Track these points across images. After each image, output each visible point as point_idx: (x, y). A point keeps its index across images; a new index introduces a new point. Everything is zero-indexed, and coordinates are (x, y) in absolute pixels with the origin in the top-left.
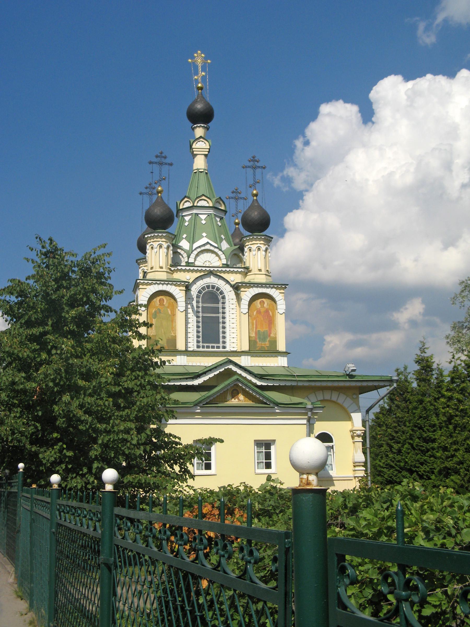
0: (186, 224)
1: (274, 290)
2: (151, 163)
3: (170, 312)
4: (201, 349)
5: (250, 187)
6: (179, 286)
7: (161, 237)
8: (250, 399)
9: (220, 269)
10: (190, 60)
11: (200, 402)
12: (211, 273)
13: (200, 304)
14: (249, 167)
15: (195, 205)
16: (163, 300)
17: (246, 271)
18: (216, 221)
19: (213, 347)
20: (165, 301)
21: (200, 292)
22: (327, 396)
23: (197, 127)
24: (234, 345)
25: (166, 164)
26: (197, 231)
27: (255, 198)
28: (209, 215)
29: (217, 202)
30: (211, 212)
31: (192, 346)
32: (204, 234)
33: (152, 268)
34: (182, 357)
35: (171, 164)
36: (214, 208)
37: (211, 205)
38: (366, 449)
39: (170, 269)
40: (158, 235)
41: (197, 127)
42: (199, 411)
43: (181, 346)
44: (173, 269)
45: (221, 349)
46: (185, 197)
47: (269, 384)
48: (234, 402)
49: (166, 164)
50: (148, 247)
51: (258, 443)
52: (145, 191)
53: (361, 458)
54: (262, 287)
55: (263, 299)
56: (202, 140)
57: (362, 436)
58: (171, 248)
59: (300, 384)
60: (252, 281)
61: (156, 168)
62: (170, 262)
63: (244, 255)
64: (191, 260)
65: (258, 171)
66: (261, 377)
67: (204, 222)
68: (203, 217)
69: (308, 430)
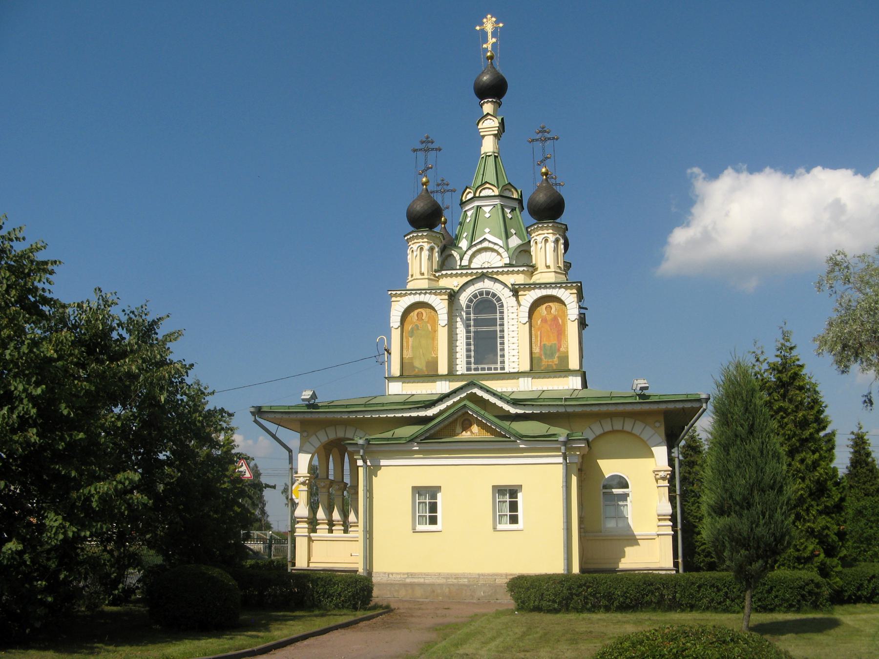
1: (563, 290)
4: (473, 372)
6: (440, 294)
7: (422, 237)
10: (478, 28)
11: (416, 437)
12: (482, 276)
13: (472, 315)
15: (477, 195)
17: (531, 269)
19: (489, 369)
20: (424, 315)
21: (471, 301)
24: (513, 365)
28: (494, 206)
30: (497, 202)
34: (444, 382)
36: (501, 196)
38: (675, 498)
39: (435, 276)
43: (443, 369)
44: (437, 275)
45: (499, 371)
46: (467, 188)
48: (466, 435)
50: (409, 251)
51: (500, 490)
53: (668, 509)
54: (546, 288)
59: (570, 410)
60: (538, 282)
62: (435, 267)
66: (515, 403)
67: (487, 215)
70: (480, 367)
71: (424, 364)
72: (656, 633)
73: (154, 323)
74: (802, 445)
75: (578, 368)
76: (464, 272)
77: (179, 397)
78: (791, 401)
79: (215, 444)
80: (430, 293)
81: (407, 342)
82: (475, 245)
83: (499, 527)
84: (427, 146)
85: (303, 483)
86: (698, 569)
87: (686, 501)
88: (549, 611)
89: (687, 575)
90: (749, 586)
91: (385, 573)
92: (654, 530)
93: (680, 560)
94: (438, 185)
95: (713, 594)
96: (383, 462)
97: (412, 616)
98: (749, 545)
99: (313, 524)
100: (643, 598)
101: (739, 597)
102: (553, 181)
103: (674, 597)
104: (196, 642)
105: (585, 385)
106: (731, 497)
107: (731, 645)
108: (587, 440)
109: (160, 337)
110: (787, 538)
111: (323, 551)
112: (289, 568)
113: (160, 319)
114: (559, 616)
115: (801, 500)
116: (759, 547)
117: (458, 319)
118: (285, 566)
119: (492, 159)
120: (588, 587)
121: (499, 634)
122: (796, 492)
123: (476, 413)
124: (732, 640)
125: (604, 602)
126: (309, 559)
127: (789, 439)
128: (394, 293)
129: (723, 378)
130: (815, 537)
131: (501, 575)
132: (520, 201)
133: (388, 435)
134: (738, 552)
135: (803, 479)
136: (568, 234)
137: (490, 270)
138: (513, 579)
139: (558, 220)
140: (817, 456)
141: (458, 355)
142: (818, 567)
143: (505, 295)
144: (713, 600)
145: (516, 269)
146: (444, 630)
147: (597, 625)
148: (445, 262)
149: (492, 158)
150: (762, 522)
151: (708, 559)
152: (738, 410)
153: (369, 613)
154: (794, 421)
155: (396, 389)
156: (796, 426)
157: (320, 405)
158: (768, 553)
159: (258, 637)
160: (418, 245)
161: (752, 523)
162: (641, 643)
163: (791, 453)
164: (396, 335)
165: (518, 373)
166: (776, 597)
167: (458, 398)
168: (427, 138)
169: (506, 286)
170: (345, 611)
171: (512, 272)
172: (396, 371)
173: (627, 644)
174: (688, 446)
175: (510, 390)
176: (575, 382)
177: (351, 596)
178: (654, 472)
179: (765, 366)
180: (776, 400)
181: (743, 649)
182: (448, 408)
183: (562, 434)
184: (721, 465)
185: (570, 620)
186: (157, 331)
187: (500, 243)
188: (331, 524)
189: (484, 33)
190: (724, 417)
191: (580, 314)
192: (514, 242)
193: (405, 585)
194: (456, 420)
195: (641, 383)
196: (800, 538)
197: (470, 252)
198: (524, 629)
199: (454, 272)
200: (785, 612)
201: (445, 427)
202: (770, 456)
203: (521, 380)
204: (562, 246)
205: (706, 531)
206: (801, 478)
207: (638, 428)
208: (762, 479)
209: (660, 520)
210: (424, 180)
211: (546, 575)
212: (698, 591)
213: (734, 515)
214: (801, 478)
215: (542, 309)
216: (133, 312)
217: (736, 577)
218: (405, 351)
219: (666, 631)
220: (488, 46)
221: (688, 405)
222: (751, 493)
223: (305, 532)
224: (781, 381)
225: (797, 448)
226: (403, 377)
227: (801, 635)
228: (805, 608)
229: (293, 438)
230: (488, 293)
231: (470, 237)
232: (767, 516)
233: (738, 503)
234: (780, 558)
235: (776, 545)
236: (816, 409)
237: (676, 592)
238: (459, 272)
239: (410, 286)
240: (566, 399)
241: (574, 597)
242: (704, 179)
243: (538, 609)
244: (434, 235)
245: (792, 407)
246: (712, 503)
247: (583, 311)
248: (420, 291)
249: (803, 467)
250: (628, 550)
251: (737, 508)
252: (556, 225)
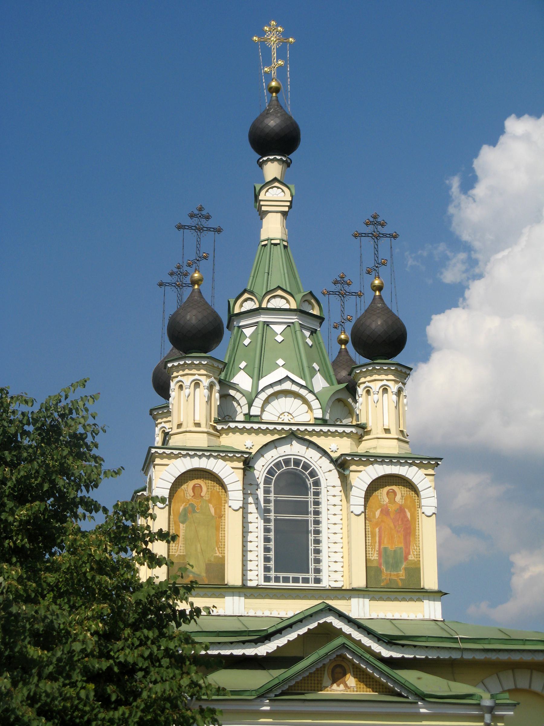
0: (247, 342)
1: (414, 468)
2: (180, 227)
3: (212, 511)
4: (272, 583)
5: (369, 273)
6: (231, 460)
7: (198, 367)
9: (310, 428)
10: (255, 38)
11: (270, 690)
12: (293, 436)
13: (272, 495)
14: (366, 235)
15: (264, 305)
17: (360, 431)
18: (304, 337)
19: (296, 580)
20: (204, 489)
21: (271, 472)
24: (338, 576)
25: (209, 229)
26: (267, 355)
29: (305, 300)
30: (294, 319)
31: (256, 578)
32: (280, 362)
33: (179, 426)
34: (236, 598)
35: (218, 230)
36: (299, 311)
37: (294, 306)
39: (215, 428)
41: (268, 160)
42: (268, 708)
43: (233, 577)
44: (219, 427)
45: (312, 585)
46: (245, 291)
47: (406, 656)
48: (336, 690)
49: (209, 229)
52: (188, 222)
54: (391, 463)
55: (394, 487)
56: (277, 184)
58: (217, 387)
59: (468, 656)
60: (372, 452)
61: (190, 235)
62: (214, 415)
63: (356, 401)
64: (255, 411)
65: (384, 242)
66: (389, 641)
67: (279, 338)
68: (278, 329)
71: (203, 567)
80: (216, 457)
160: (192, 378)
168: (201, 209)
210: (196, 275)
215: (383, 494)
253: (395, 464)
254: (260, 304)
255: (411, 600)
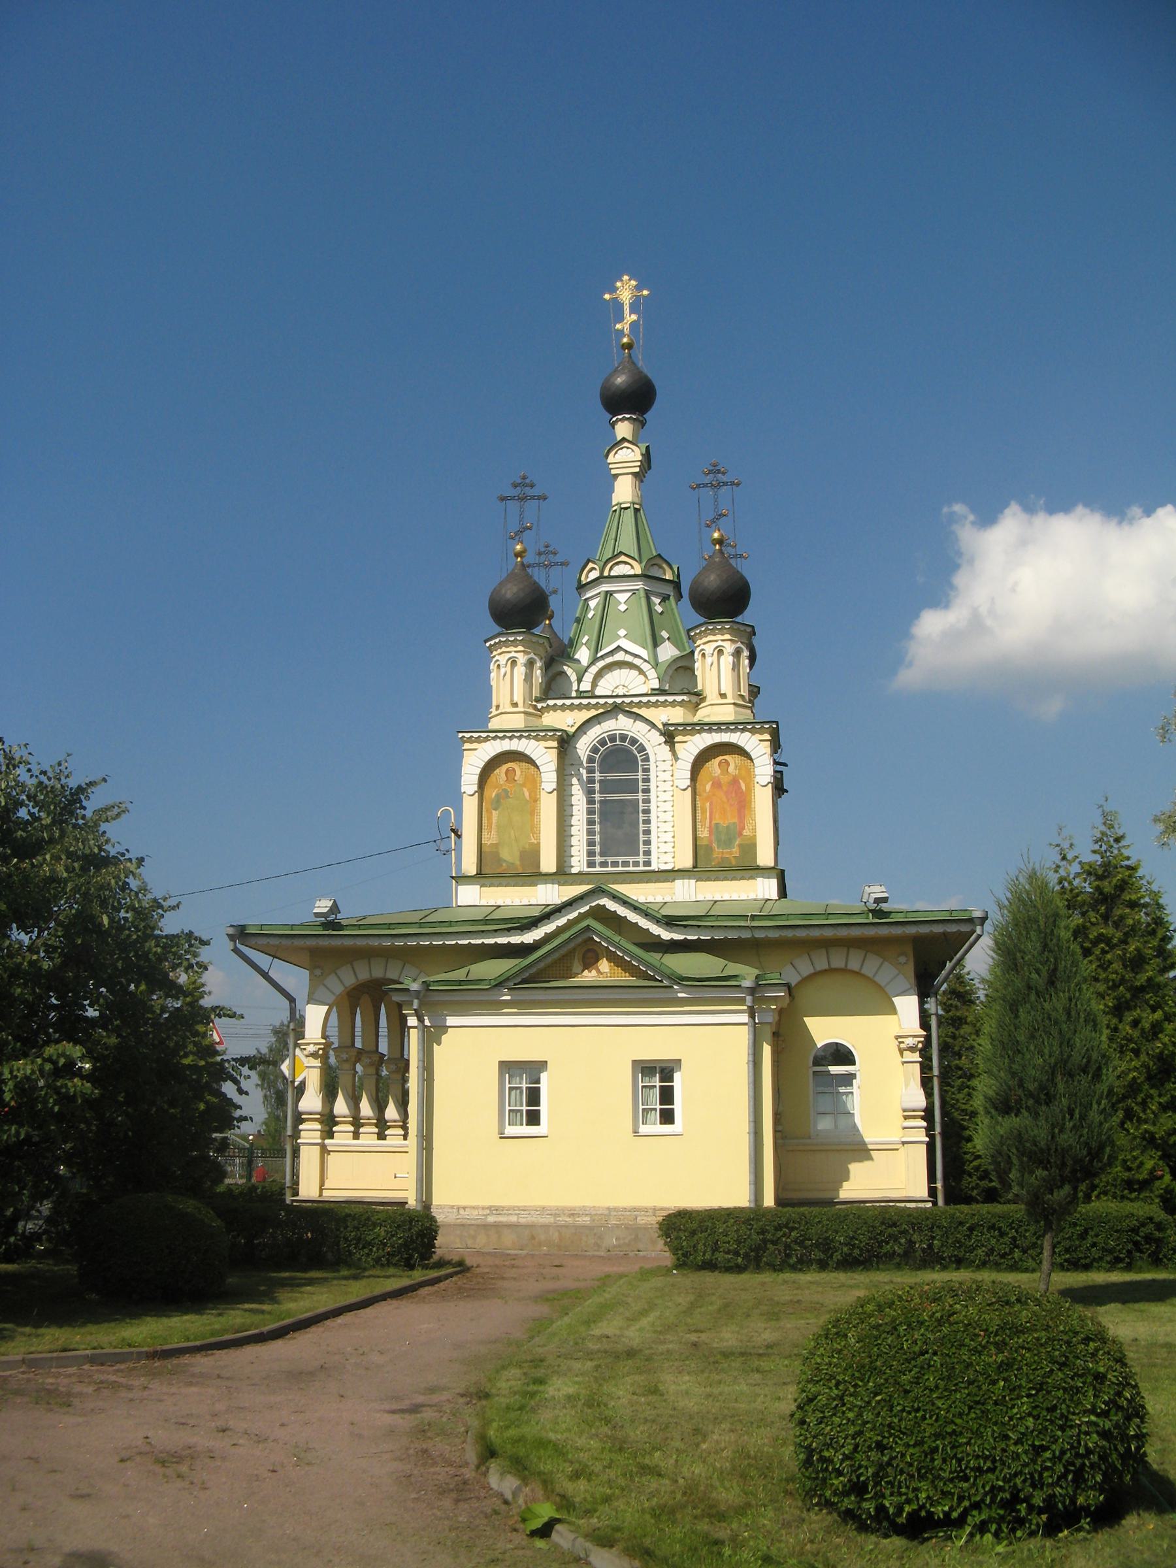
1: (747, 734)
3: (527, 794)
4: (598, 869)
5: (708, 526)
6: (544, 738)
7: (514, 643)
8: (625, 970)
10: (607, 296)
11: (508, 979)
12: (615, 710)
13: (640, 777)
15: (606, 574)
16: (514, 770)
17: (694, 699)
19: (625, 864)
20: (518, 772)
21: (595, 750)
22: (838, 963)
23: (617, 421)
24: (664, 858)
25: (533, 498)
26: (609, 625)
27: (717, 547)
28: (634, 592)
30: (639, 585)
36: (644, 576)
37: (639, 572)
38: (930, 1079)
39: (535, 707)
40: (507, 640)
41: (617, 421)
42: (509, 998)
43: (548, 864)
44: (539, 706)
45: (641, 868)
46: (588, 561)
47: (689, 938)
50: (492, 666)
51: (645, 1068)
52: (511, 492)
53: (920, 1100)
54: (719, 730)
56: (626, 444)
57: (921, 1050)
59: (760, 934)
60: (707, 720)
61: (513, 506)
62: (536, 692)
66: (670, 922)
67: (623, 607)
69: (752, 1037)
70: (610, 860)
71: (518, 854)
72: (912, 1292)
73: (80, 789)
74: (1134, 996)
75: (772, 865)
76: (585, 702)
77: (123, 914)
78: (1116, 925)
79: (174, 990)
80: (528, 737)
81: (490, 819)
82: (602, 657)
83: (643, 1129)
84: (523, 492)
85: (314, 1055)
86: (968, 1200)
87: (949, 1085)
88: (728, 1270)
89: (952, 1209)
90: (1049, 1227)
91: (452, 1207)
92: (896, 1136)
93: (939, 1185)
94: (540, 554)
95: (993, 1242)
96: (451, 1021)
97: (503, 1278)
98: (1049, 1162)
99: (329, 1122)
100: (881, 1247)
101: (1034, 1246)
102: (732, 551)
103: (930, 1246)
104: (165, 1320)
105: (783, 893)
106: (1021, 1085)
107: (1017, 1307)
108: (788, 985)
109: (89, 813)
110: (1108, 1149)
111: (345, 1168)
112: (289, 1199)
113: (91, 784)
114: (744, 1277)
115: (1133, 1088)
116: (1064, 1164)
117: (575, 781)
118: (282, 1193)
119: (630, 514)
120: (793, 1229)
121: (652, 1306)
122: (1124, 1074)
123: (607, 939)
124: (1018, 1300)
125: (817, 1254)
126: (322, 1184)
127: (1115, 987)
128: (468, 735)
129: (1009, 895)
130: (1157, 1148)
131: (646, 1210)
132: (676, 584)
133: (460, 974)
134: (1031, 1172)
135: (1137, 1052)
136: (756, 641)
137: (627, 700)
138: (669, 1215)
139: (739, 619)
140: (1158, 1015)
141: (574, 841)
142: (1161, 1196)
143: (653, 742)
144: (992, 1250)
145: (670, 698)
146: (561, 1299)
147: (807, 1292)
148: (553, 686)
149: (630, 512)
150: (1069, 1125)
151: (984, 1184)
152: (1032, 946)
153: (434, 1274)
154: (1122, 958)
155: (469, 896)
156: (1125, 966)
157: (344, 923)
158: (1079, 1175)
159: (263, 1312)
161: (1053, 1126)
162: (891, 1305)
163: (1119, 1010)
164: (470, 806)
165: (672, 871)
166: (1094, 1245)
167: (575, 914)
168: (524, 478)
169: (653, 725)
170: (392, 1271)
171: (665, 704)
172: (469, 865)
173: (870, 1308)
174: (953, 992)
175: (659, 899)
176: (767, 888)
177: (402, 1244)
178: (897, 1037)
179: (1075, 868)
180: (1093, 924)
181: (1034, 1313)
182: (560, 931)
183: (747, 974)
184: (1006, 1033)
185: (763, 1284)
186: (85, 803)
187: (644, 653)
188: (357, 1122)
189: (617, 305)
190: (1009, 955)
191: (775, 772)
192: (668, 652)
193: (486, 1227)
194: (572, 952)
195: (877, 891)
196: (1132, 1150)
197: (594, 670)
198: (691, 1298)
199: (568, 702)
200: (1108, 1271)
201: (555, 962)
202: (1082, 1020)
203: (678, 883)
204: (747, 662)
205: (981, 1140)
206: (1133, 1050)
207: (871, 966)
208: (1070, 1056)
209: (906, 1118)
210: (518, 547)
211: (721, 1210)
212: (969, 1237)
213: (1026, 1114)
214: (1133, 1050)
215: (714, 766)
216: (44, 773)
217: (1029, 1214)
218: (485, 833)
219: (926, 1288)
220: (624, 326)
221: (952, 928)
222: (1052, 1079)
223: (316, 1137)
224: (1101, 893)
225: (1127, 1002)
226: (481, 877)
227: (1131, 1305)
228: (1139, 1263)
229: (294, 978)
230: (623, 738)
231: (593, 644)
232: (1077, 1116)
233: (1031, 1095)
234: (1102, 1180)
235: (1091, 1161)
236: (1160, 935)
237: (933, 1238)
238: (577, 702)
239: (494, 724)
240: (753, 917)
241: (770, 1246)
242: (973, 523)
243: (709, 1266)
244: (535, 639)
245: (1119, 934)
246: (991, 1093)
247: (779, 768)
248: (511, 733)
249: (1136, 1034)
250: (854, 1168)
251: (1031, 1102)
252: (736, 626)
253: (726, 731)
254: (602, 571)
255: (742, 878)
